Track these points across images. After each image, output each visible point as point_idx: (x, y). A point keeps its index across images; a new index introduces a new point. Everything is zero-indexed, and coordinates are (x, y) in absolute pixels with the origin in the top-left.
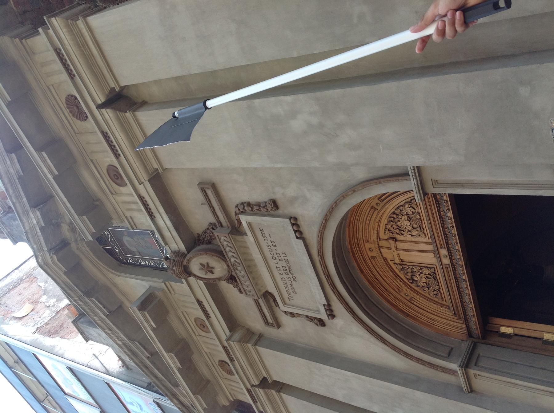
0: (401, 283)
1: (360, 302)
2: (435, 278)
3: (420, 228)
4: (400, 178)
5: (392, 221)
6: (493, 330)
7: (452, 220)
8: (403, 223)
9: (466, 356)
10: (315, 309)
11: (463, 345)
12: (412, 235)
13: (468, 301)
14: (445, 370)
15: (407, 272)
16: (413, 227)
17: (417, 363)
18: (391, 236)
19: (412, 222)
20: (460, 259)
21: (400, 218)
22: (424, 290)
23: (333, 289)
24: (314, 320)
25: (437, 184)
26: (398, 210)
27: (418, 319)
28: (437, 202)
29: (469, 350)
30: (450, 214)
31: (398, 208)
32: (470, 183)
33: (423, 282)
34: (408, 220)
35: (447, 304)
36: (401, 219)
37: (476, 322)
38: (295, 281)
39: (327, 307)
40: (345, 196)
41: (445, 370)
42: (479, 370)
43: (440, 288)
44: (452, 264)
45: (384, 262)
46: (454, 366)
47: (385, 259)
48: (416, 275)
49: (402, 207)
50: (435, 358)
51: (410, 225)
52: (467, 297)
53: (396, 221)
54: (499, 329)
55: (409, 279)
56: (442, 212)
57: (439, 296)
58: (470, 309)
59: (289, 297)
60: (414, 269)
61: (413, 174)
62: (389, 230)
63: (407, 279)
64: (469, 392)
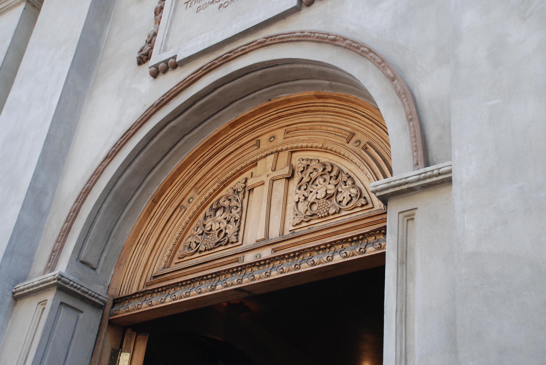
0: (211, 190)
1: (180, 118)
2: (218, 244)
3: (310, 214)
4: (420, 153)
5: (324, 169)
6: (125, 340)
7: (326, 262)
8: (321, 187)
9: (79, 289)
10: (169, 45)
11: (101, 287)
12: (297, 202)
13: (177, 294)
14: (56, 253)
15: (230, 200)
16: (313, 203)
17: (71, 210)
18: (296, 170)
19: (322, 202)
20: (254, 279)
21: (331, 182)
22: (198, 228)
23: (203, 69)
24: (149, 45)
25: (406, 219)
26: (347, 178)
27: (147, 218)
28: (361, 237)
29: (90, 295)
30: (338, 259)
31: (349, 177)
32: (408, 276)
33: (212, 226)
34: (327, 194)
35: (173, 264)
36: (329, 183)
37: (139, 309)
38: (220, 7)
39: (171, 64)
40: (383, 65)
41: (56, 253)
42: (52, 308)
43: (200, 252)
44: (244, 267)
45: (249, 162)
46: (62, 267)
47: (254, 164)
48: (224, 214)
49: (352, 184)
50: (77, 238)
51: (316, 198)
52: (184, 293)
53: (325, 176)
54: (126, 351)
55: (218, 203)
56: (342, 247)
57: (187, 251)
58: (162, 299)
59: (190, 3)
60: (236, 209)
61: (428, 174)
62: (308, 165)
63: (219, 200)
64: (14, 293)
